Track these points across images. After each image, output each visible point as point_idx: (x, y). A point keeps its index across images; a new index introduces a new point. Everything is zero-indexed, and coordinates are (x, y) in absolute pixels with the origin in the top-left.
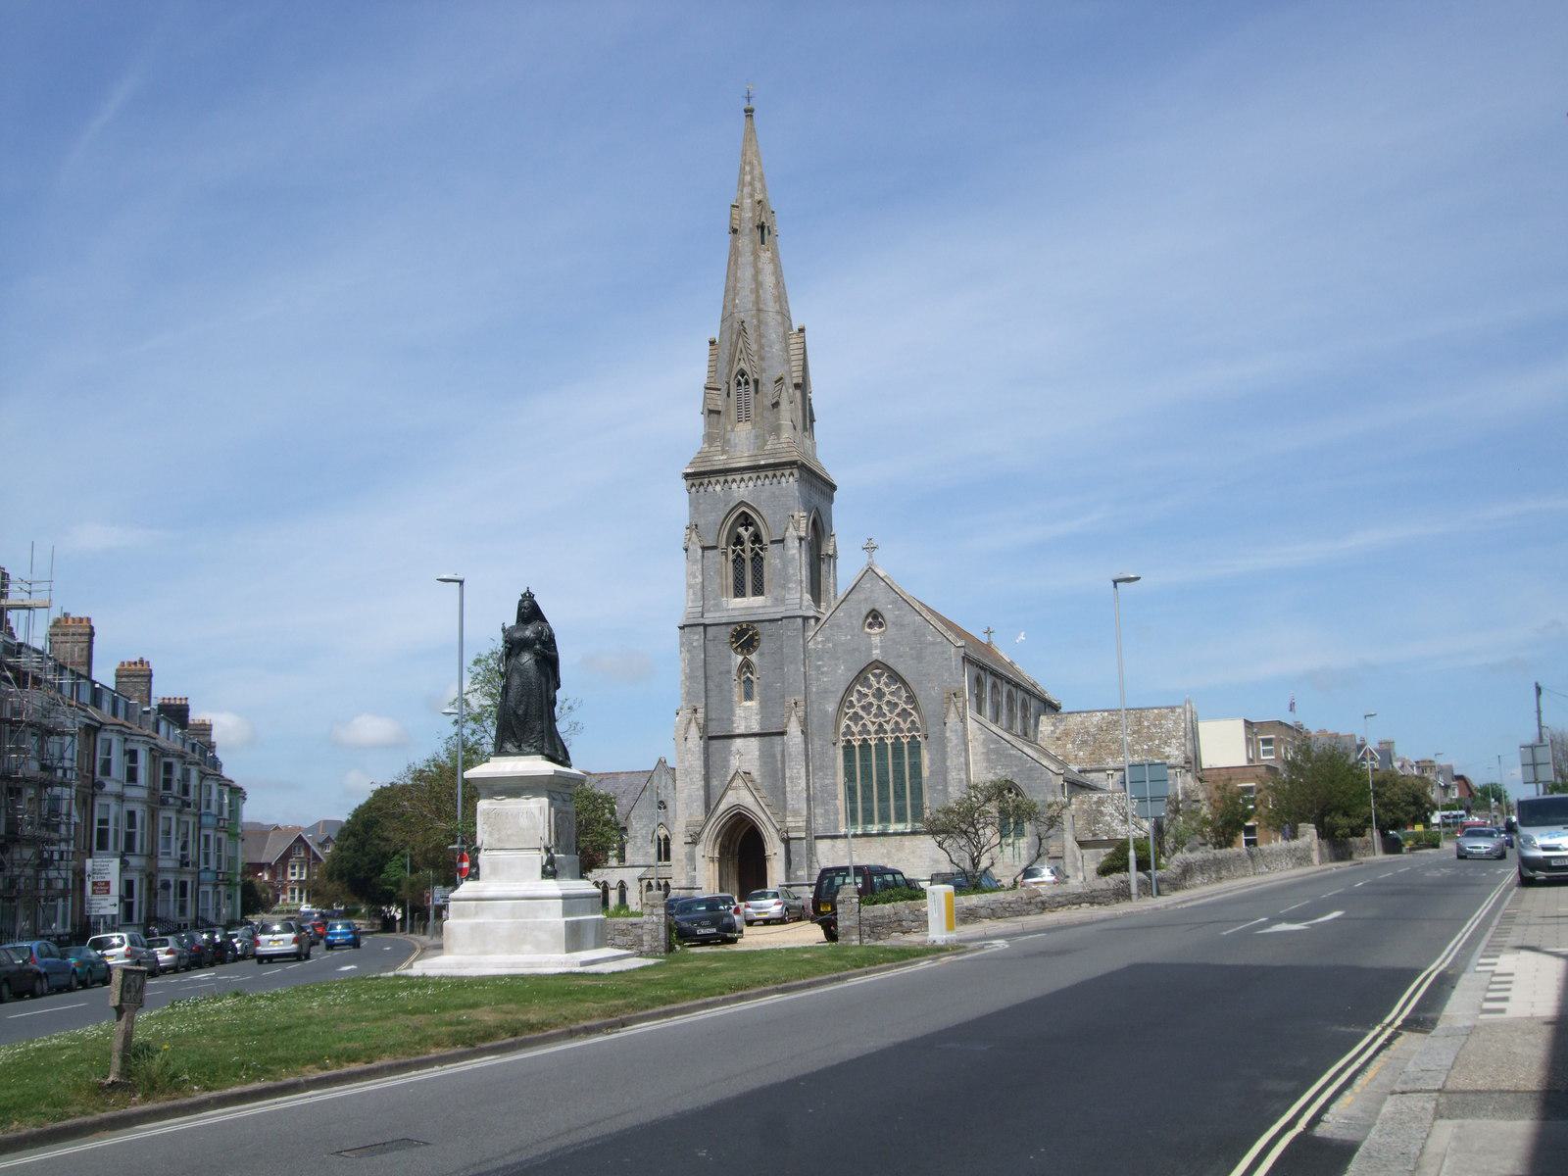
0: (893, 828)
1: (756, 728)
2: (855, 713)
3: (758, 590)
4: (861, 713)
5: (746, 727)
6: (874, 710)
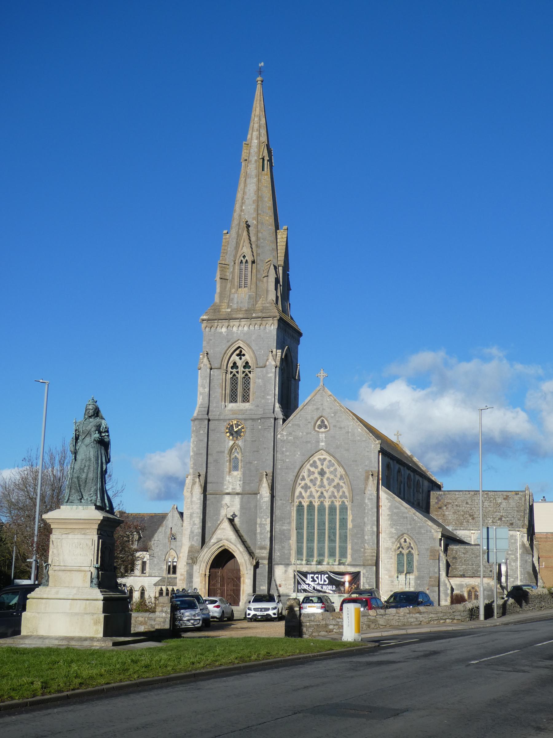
1: (239, 490)
2: (306, 484)
3: (246, 399)
4: (309, 484)
5: (233, 489)
6: (318, 483)
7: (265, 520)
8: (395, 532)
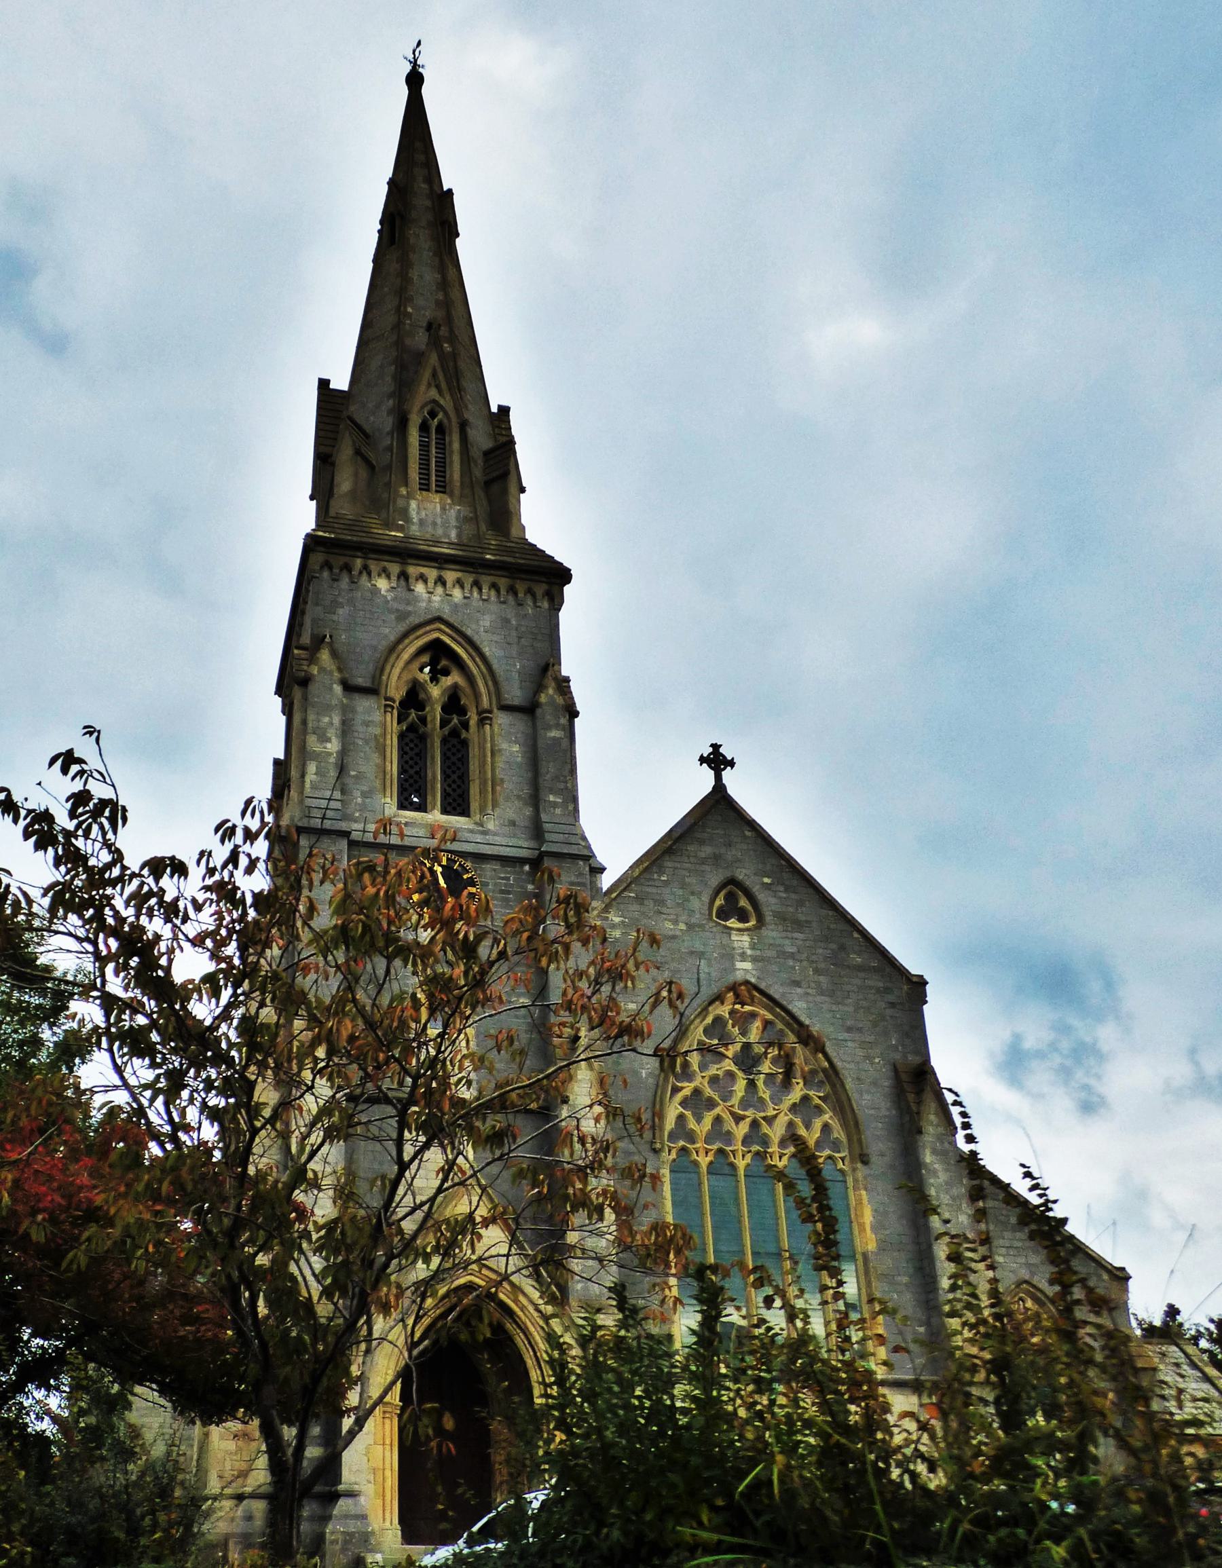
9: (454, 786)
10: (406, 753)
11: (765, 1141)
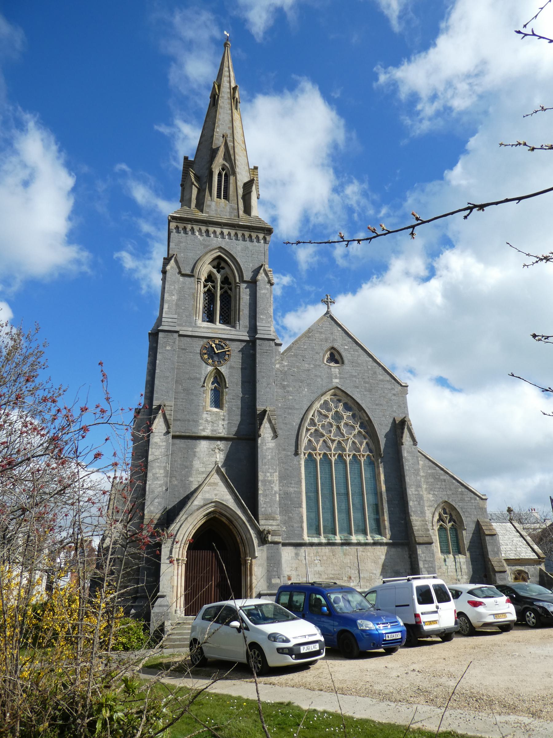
0: (354, 538)
5: (212, 431)
7: (271, 475)
8: (433, 499)
9: (225, 312)
10: (223, 301)
11: (344, 450)
